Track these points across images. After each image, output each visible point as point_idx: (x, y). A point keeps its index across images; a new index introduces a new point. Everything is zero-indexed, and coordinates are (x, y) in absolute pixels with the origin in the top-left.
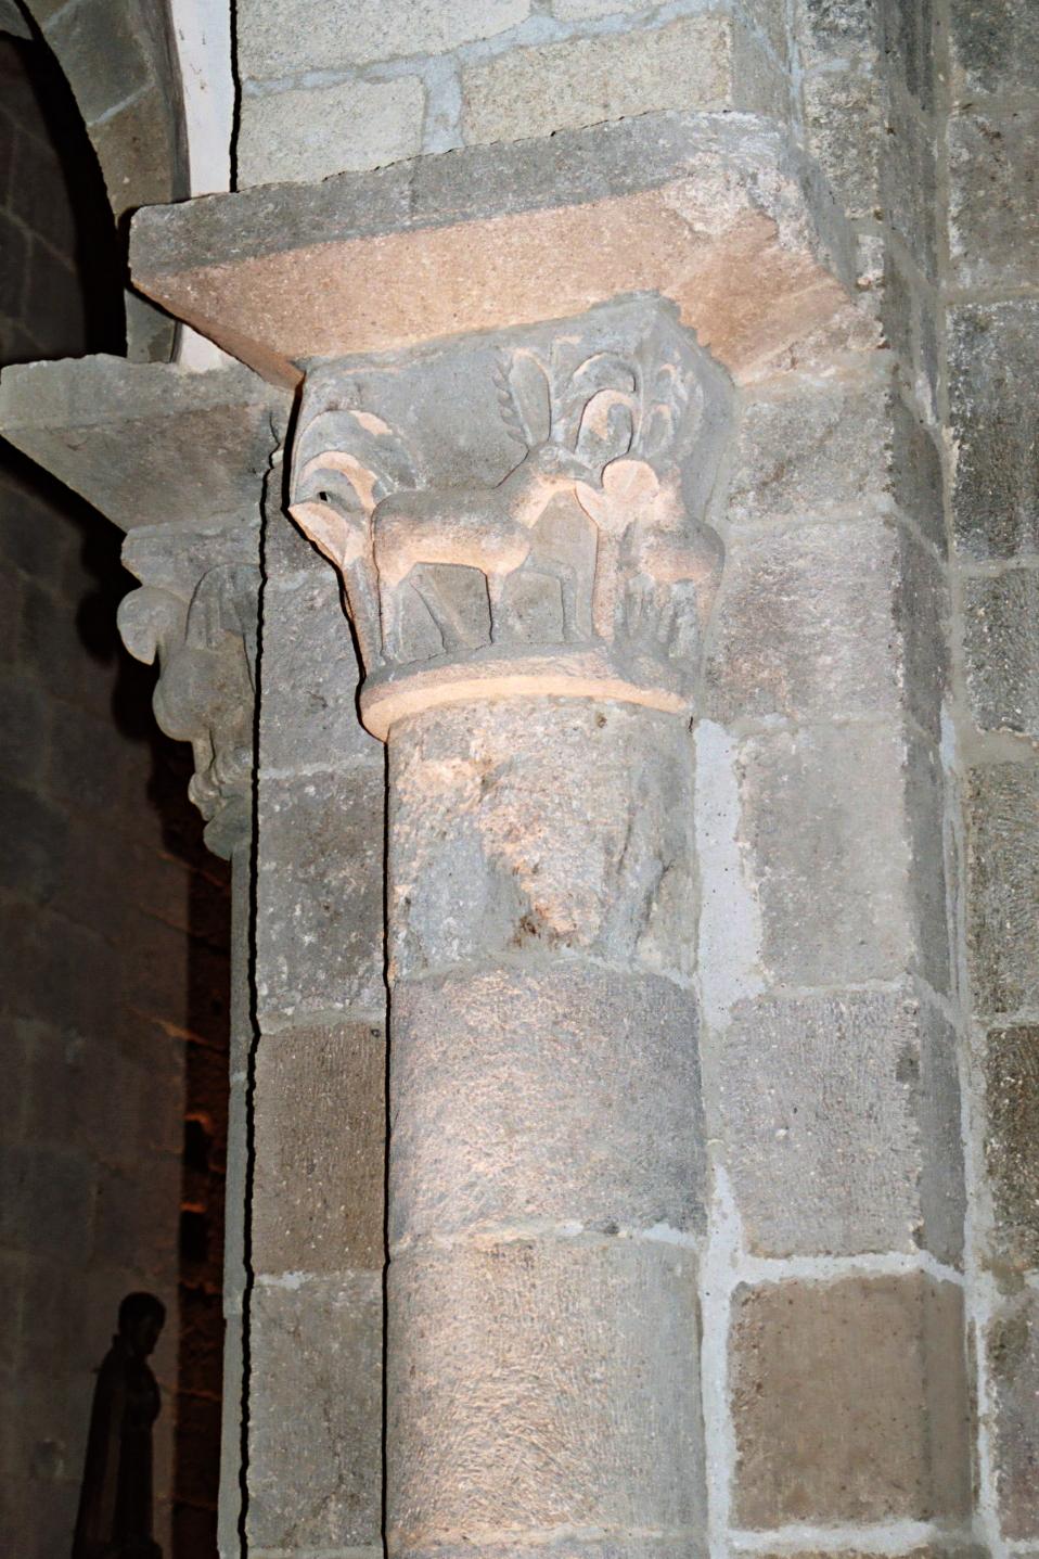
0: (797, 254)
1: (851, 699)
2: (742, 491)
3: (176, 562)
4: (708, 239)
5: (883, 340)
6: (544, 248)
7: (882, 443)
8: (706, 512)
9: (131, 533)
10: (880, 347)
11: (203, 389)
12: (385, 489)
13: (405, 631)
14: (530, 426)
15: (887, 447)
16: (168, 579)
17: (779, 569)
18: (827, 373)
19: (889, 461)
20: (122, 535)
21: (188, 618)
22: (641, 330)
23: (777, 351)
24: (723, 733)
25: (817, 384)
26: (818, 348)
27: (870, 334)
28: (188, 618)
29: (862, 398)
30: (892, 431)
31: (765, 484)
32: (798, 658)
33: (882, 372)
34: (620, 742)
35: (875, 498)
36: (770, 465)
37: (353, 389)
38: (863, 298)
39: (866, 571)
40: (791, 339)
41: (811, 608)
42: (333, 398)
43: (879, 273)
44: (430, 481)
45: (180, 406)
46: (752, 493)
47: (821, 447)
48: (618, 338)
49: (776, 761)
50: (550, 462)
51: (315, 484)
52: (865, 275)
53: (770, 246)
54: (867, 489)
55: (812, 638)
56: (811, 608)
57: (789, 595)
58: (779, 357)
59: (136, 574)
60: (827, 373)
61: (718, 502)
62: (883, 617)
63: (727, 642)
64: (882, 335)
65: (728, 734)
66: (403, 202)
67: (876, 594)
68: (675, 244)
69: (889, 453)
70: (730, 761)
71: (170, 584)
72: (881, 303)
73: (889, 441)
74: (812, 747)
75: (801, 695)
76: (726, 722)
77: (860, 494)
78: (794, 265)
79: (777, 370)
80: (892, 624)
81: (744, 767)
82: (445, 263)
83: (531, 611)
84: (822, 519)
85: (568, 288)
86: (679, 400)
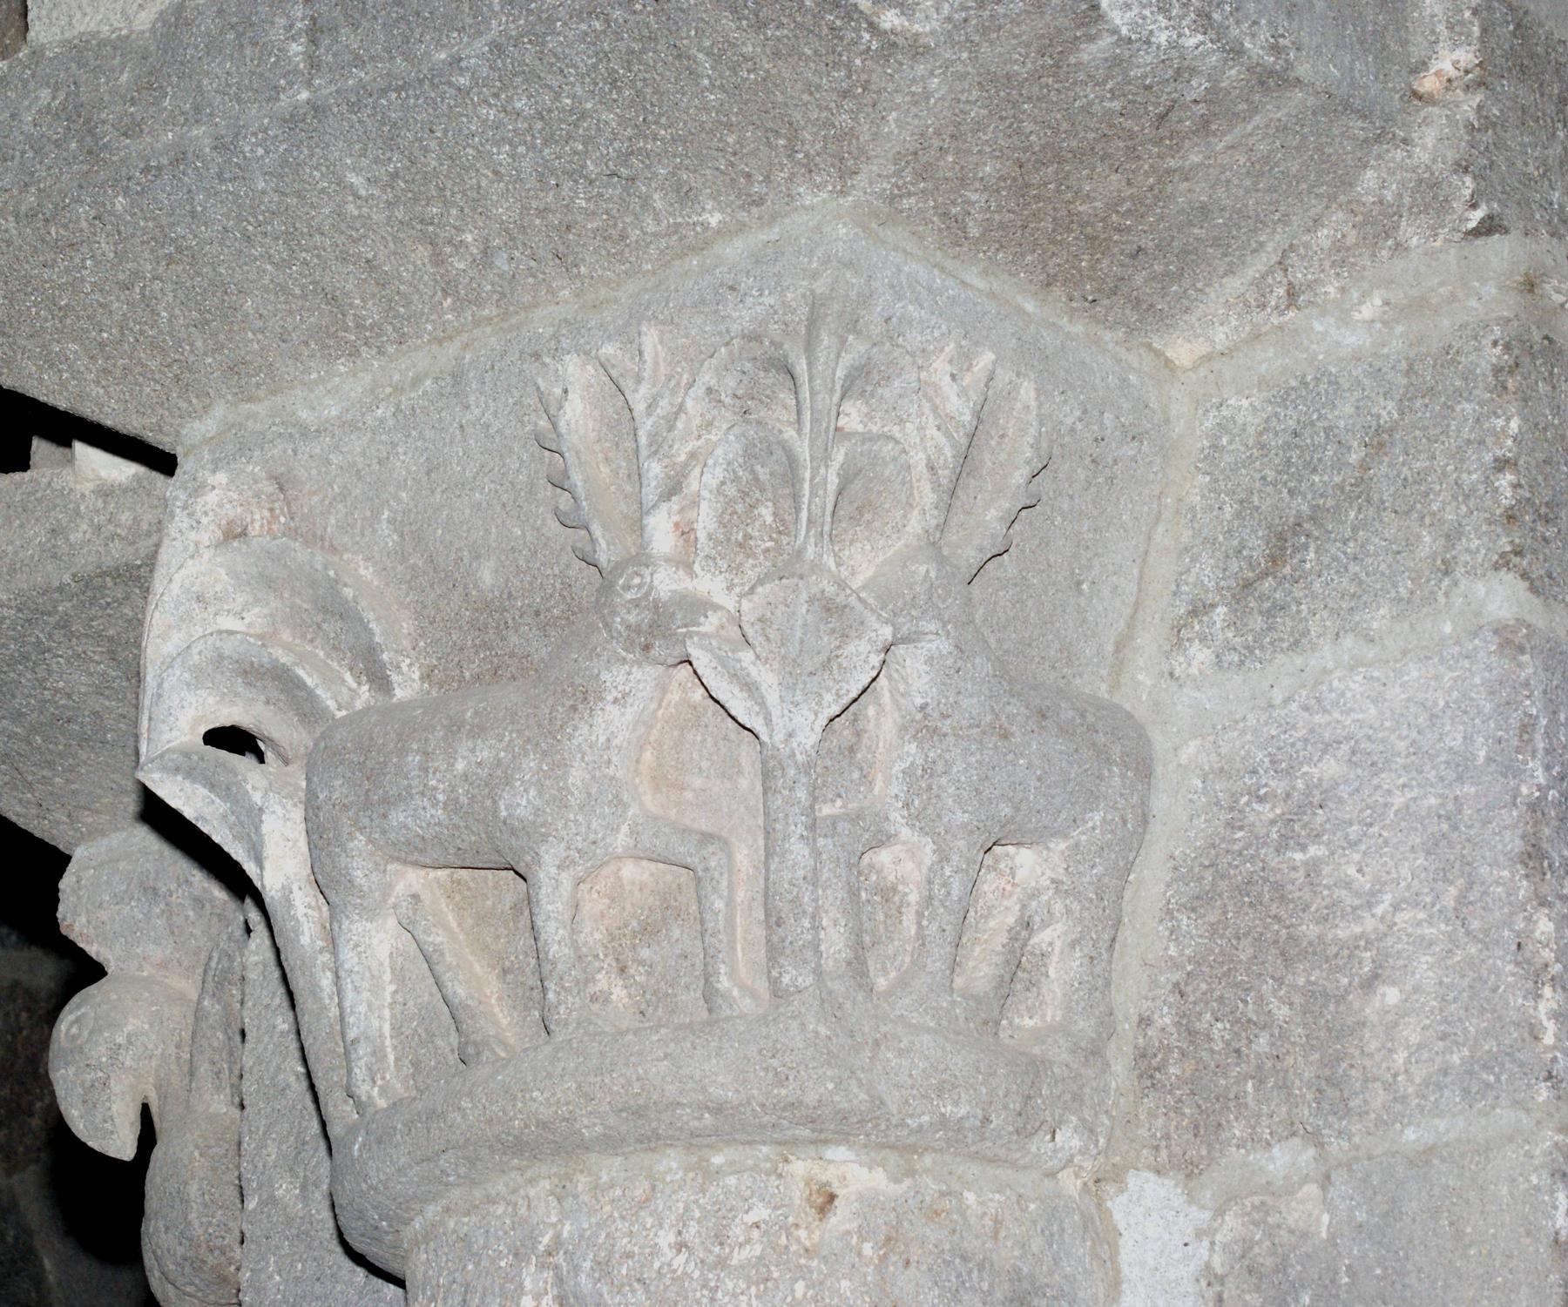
0: (1173, 45)
1: (1440, 1087)
2: (1199, 610)
3: (169, 913)
4: (917, 49)
5: (1477, 215)
6: (584, 115)
7: (1488, 458)
8: (1118, 665)
9: (79, 854)
10: (1476, 233)
11: (126, 517)
12: (331, 704)
13: (397, 1030)
14: (606, 527)
15: (1502, 465)
16: (156, 953)
17: (1279, 786)
18: (1366, 312)
19: (1507, 497)
20: (59, 861)
21: (302, 1049)
22: (814, 275)
23: (1251, 273)
24: (1179, 1200)
25: (1352, 339)
26: (1341, 255)
27: (1444, 206)
28: (302, 1049)
29: (1448, 356)
30: (1514, 424)
31: (1247, 585)
32: (1326, 996)
33: (1490, 290)
34: (867, 1248)
35: (1480, 588)
36: (1257, 548)
37: (269, 488)
38: (1426, 122)
39: (1462, 767)
40: (1273, 243)
41: (1352, 871)
42: (231, 512)
43: (1466, 56)
44: (427, 677)
45: (84, 563)
46: (1221, 610)
47: (1360, 490)
48: (769, 300)
49: (1285, 1258)
50: (636, 604)
51: (190, 713)
52: (1435, 66)
53: (1092, 39)
54: (1459, 572)
55: (1353, 946)
56: (1352, 871)
57: (1303, 848)
58: (1260, 285)
59: (93, 950)
60: (1366, 312)
61: (1149, 640)
62: (1503, 878)
63: (1177, 976)
64: (1474, 206)
65: (1191, 1199)
66: (295, 48)
67: (1485, 823)
68: (849, 67)
69: (1506, 480)
70: (1194, 1267)
71: (163, 965)
72: (1470, 128)
73: (1508, 447)
74: (1361, 1216)
75: (1334, 1093)
76: (1189, 1171)
77: (1446, 582)
78: (1184, 72)
79: (1259, 317)
80: (1524, 889)
81: (1221, 1280)
82: (395, 176)
83: (645, 953)
84: (1371, 653)
85: (658, 201)
86: (945, 423)
